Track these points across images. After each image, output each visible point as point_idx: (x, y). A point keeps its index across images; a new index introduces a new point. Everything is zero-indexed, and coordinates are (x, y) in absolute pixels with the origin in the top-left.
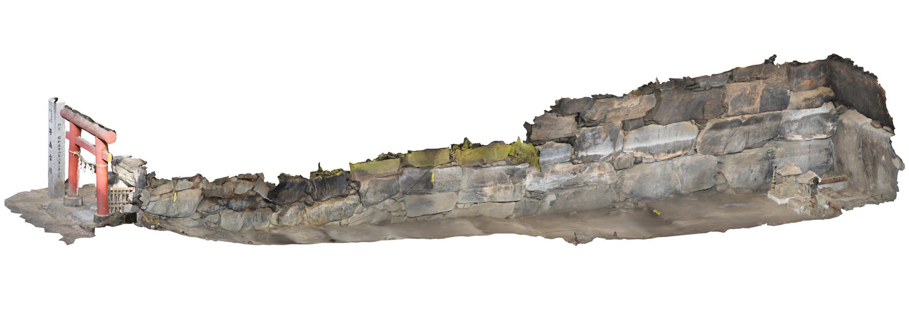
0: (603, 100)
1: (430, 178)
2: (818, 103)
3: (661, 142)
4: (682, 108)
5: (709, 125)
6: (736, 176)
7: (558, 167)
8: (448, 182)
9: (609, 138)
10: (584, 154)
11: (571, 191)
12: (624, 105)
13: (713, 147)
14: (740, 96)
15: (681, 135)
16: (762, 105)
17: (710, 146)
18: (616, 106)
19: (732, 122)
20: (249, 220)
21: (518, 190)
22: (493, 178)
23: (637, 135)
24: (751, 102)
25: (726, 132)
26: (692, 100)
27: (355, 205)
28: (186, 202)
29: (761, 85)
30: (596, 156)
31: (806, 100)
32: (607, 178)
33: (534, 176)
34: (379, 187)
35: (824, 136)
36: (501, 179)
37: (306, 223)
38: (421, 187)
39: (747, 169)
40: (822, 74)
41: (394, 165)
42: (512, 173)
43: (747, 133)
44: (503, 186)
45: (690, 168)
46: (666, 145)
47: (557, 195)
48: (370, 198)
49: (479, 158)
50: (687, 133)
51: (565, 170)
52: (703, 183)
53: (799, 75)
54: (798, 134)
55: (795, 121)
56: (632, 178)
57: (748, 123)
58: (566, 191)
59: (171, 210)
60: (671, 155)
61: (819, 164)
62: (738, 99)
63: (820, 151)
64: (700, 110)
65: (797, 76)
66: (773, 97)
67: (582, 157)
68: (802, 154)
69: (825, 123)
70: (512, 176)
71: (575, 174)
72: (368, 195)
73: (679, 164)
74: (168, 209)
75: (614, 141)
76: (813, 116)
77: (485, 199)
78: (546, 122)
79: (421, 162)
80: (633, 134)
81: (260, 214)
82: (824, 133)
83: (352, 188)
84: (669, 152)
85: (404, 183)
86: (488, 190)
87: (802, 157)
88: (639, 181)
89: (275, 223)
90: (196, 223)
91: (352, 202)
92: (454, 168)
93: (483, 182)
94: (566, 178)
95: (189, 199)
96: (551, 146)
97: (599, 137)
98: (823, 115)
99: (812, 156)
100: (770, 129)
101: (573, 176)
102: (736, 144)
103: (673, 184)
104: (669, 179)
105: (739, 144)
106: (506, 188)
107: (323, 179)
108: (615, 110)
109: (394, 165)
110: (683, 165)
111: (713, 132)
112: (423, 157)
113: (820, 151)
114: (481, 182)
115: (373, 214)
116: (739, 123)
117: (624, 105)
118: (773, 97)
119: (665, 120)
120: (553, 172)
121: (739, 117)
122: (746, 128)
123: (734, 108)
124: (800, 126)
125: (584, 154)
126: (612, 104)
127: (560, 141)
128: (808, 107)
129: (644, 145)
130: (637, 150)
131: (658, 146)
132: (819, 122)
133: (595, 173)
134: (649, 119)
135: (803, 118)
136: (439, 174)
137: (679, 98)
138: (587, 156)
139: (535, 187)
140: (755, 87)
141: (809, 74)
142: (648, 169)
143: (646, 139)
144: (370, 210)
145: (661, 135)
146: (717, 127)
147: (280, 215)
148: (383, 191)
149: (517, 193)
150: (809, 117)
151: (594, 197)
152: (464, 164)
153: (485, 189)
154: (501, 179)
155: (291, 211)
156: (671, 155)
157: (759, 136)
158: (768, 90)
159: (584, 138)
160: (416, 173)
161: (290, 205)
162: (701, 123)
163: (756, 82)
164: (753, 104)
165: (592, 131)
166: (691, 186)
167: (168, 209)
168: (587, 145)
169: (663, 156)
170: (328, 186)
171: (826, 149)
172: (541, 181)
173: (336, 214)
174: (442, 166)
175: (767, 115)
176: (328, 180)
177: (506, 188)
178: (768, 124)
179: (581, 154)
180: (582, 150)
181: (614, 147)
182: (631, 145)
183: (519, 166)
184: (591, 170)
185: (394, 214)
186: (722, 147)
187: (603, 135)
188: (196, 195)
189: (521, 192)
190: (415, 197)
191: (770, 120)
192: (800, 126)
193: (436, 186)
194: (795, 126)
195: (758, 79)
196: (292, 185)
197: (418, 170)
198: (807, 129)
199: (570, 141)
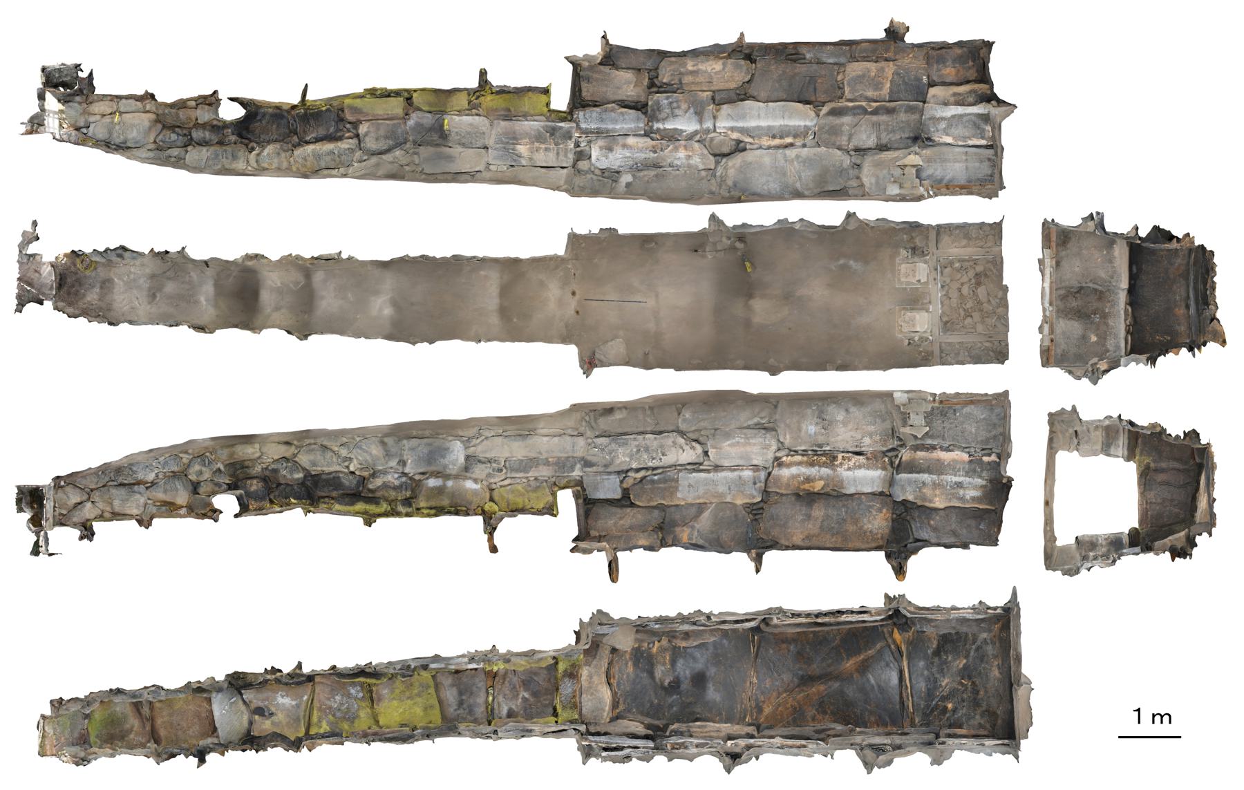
0: (673, 59)
1: (442, 126)
2: (971, 100)
3: (764, 123)
4: (784, 83)
5: (825, 110)
6: (873, 180)
7: (631, 141)
8: (469, 133)
9: (692, 110)
10: (660, 126)
11: (652, 173)
12: (702, 67)
13: (833, 138)
14: (863, 76)
15: (790, 117)
16: (891, 91)
17: (826, 137)
18: (690, 68)
19: (854, 108)
20: (217, 155)
21: (562, 154)
22: (527, 135)
23: (730, 111)
24: (878, 86)
25: (847, 119)
26: (796, 74)
27: (352, 151)
28: (133, 126)
29: (890, 69)
30: (676, 130)
31: (955, 94)
32: (696, 161)
33: (601, 148)
34: (382, 132)
35: (984, 142)
36: (539, 138)
37: (294, 169)
38: (435, 137)
39: (885, 172)
40: (971, 63)
41: (396, 106)
42: (553, 131)
43: (876, 125)
44: (543, 146)
45: (807, 162)
46: (769, 128)
47: (634, 176)
48: (370, 144)
49: (503, 106)
50: (801, 118)
51: (640, 145)
52: (826, 182)
53: (941, 60)
54: (947, 135)
55: (943, 119)
56: (733, 166)
57: (875, 112)
58: (646, 173)
59: (115, 135)
60: (777, 142)
61: (980, 176)
62: (860, 79)
63: (981, 161)
64: (811, 89)
65: (938, 62)
66: (905, 83)
67: (658, 129)
68: (956, 161)
69: (983, 126)
70: (552, 134)
71: (655, 152)
72: (367, 139)
73: (793, 156)
74: (110, 133)
75: (700, 115)
76: (966, 115)
77: (524, 163)
78: (595, 76)
79: (430, 104)
80: (726, 109)
81: (229, 149)
82: (983, 138)
83: (349, 131)
84: (774, 137)
85: (413, 129)
86: (522, 149)
87: (957, 165)
88: (741, 170)
89: (255, 165)
90: (151, 154)
91: (347, 146)
92: (477, 118)
93: (514, 138)
94: (643, 156)
95: (136, 122)
96: (613, 110)
97: (679, 107)
98: (980, 116)
99: (970, 165)
100: (908, 122)
101: (652, 155)
102: (864, 137)
103: (790, 181)
104: (784, 174)
105: (869, 137)
106: (546, 149)
107: (306, 114)
108: (692, 73)
109: (396, 106)
110: (798, 157)
111: (831, 118)
112: (431, 98)
113: (981, 161)
114: (514, 138)
115: (378, 165)
116: (865, 112)
117: (702, 67)
118: (905, 83)
119: (763, 95)
120: (624, 146)
121: (864, 104)
122: (875, 118)
123: (853, 90)
124: (950, 126)
125: (660, 126)
126: (685, 65)
127: (625, 105)
128: (958, 103)
129: (740, 124)
130: (732, 129)
131: (758, 128)
132: (975, 124)
133: (682, 154)
134: (742, 95)
135: (953, 116)
136: (456, 122)
137: (778, 69)
138: (665, 129)
139: (604, 164)
140: (882, 70)
141: (954, 61)
142: (750, 156)
143: (743, 117)
144: (374, 160)
145: (762, 115)
146: (834, 112)
147: (258, 155)
148: (387, 137)
149: (561, 157)
150: (961, 116)
151: (684, 184)
152: (491, 114)
153: (518, 147)
154: (539, 138)
155: (270, 149)
156: (777, 142)
157: (893, 131)
158: (899, 74)
159: (659, 108)
160: (428, 119)
161: (269, 142)
162: (816, 105)
163: (883, 64)
164: (881, 89)
165: (667, 98)
166: (811, 185)
167: (110, 133)
168: (663, 115)
169: (766, 142)
170: (312, 122)
171: (989, 160)
172: (610, 155)
173: (328, 158)
174: (460, 112)
175: (901, 106)
176: (312, 115)
177: (546, 149)
178: (903, 116)
179: (656, 126)
180: (658, 121)
181: (701, 122)
182: (726, 123)
183: (562, 124)
184: (676, 149)
185: (407, 168)
186: (845, 138)
187: (684, 106)
188: (145, 119)
189: (566, 156)
190: (431, 150)
191: (906, 112)
192: (950, 126)
193: (453, 137)
194: (943, 125)
195: (886, 60)
196: (264, 115)
197: (429, 115)
198: (960, 131)
199: (639, 106)
